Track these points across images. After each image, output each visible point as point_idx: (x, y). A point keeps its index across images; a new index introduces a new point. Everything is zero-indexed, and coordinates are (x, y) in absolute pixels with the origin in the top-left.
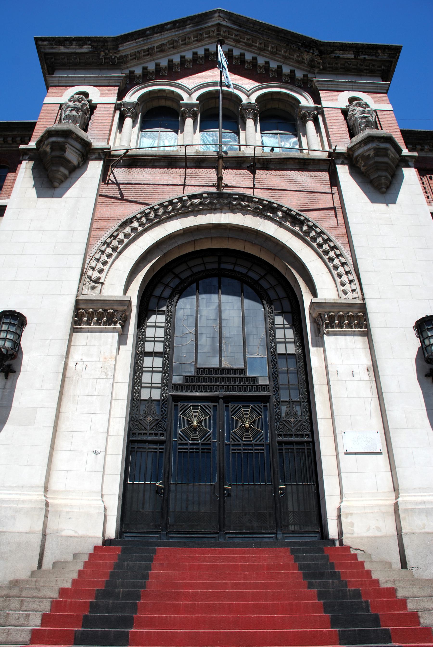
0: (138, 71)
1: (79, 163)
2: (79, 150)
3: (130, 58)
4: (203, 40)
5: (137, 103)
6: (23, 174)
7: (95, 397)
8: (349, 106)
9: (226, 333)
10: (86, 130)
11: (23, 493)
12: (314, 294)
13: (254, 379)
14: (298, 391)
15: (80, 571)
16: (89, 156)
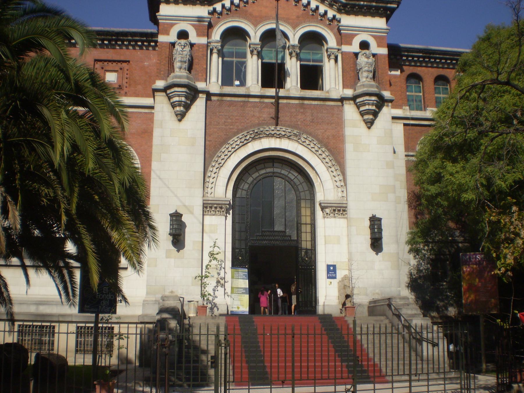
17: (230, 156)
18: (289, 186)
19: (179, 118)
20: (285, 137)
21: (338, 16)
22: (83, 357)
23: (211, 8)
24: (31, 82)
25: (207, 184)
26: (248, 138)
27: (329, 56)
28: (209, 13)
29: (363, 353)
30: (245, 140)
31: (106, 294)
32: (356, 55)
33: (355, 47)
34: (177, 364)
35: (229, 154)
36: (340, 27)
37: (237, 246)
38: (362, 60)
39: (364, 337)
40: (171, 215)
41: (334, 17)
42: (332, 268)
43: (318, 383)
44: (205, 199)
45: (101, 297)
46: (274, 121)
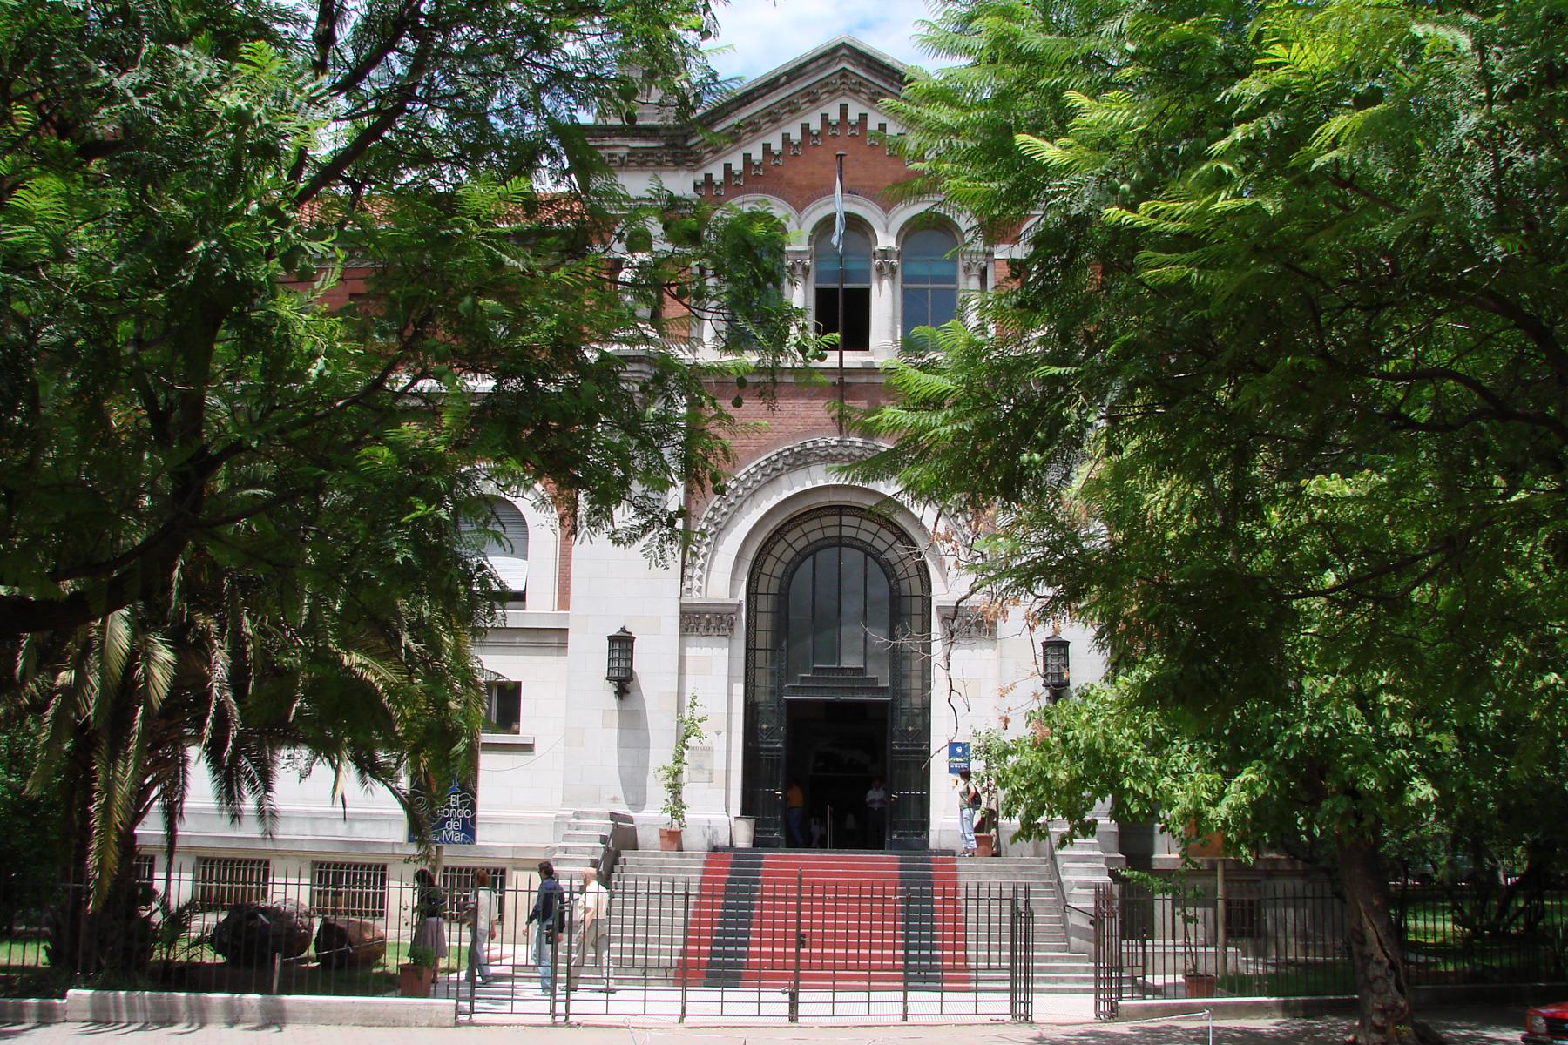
17: (741, 506)
18: (873, 567)
23: (700, 177)
24: (415, 311)
25: (688, 571)
26: (779, 465)
27: (967, 269)
28: (696, 187)
30: (773, 469)
31: (456, 808)
35: (740, 501)
37: (472, 772)
39: (972, 905)
40: (612, 639)
42: (959, 750)
43: (766, 986)
44: (686, 600)
45: (446, 813)
46: (835, 426)
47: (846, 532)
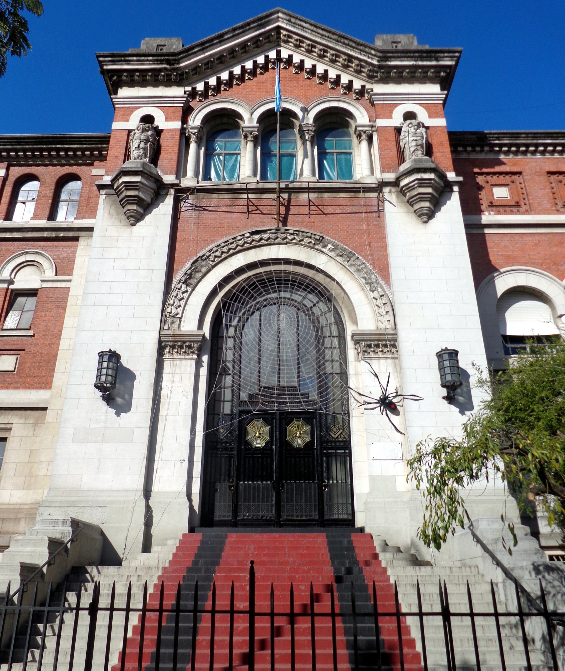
0: (200, 87)
1: (152, 199)
2: (152, 189)
3: (191, 73)
4: (263, 46)
5: (201, 127)
6: (102, 211)
7: (178, 417)
8: (403, 124)
9: (284, 357)
10: (156, 165)
11: (485, 170)
12: (355, 322)
13: (306, 395)
14: (14, 327)
15: (174, 554)
16: (160, 191)
19: (132, 222)
20: (293, 243)
21: (368, 86)
22: (470, 623)
27: (359, 136)
29: (403, 637)
32: (398, 130)
33: (397, 119)
34: (365, 623)
36: (373, 97)
38: (408, 130)
41: (363, 87)
47: (316, 310)
